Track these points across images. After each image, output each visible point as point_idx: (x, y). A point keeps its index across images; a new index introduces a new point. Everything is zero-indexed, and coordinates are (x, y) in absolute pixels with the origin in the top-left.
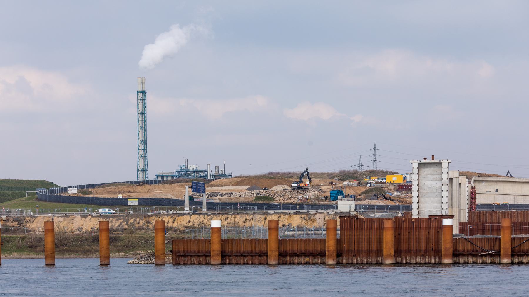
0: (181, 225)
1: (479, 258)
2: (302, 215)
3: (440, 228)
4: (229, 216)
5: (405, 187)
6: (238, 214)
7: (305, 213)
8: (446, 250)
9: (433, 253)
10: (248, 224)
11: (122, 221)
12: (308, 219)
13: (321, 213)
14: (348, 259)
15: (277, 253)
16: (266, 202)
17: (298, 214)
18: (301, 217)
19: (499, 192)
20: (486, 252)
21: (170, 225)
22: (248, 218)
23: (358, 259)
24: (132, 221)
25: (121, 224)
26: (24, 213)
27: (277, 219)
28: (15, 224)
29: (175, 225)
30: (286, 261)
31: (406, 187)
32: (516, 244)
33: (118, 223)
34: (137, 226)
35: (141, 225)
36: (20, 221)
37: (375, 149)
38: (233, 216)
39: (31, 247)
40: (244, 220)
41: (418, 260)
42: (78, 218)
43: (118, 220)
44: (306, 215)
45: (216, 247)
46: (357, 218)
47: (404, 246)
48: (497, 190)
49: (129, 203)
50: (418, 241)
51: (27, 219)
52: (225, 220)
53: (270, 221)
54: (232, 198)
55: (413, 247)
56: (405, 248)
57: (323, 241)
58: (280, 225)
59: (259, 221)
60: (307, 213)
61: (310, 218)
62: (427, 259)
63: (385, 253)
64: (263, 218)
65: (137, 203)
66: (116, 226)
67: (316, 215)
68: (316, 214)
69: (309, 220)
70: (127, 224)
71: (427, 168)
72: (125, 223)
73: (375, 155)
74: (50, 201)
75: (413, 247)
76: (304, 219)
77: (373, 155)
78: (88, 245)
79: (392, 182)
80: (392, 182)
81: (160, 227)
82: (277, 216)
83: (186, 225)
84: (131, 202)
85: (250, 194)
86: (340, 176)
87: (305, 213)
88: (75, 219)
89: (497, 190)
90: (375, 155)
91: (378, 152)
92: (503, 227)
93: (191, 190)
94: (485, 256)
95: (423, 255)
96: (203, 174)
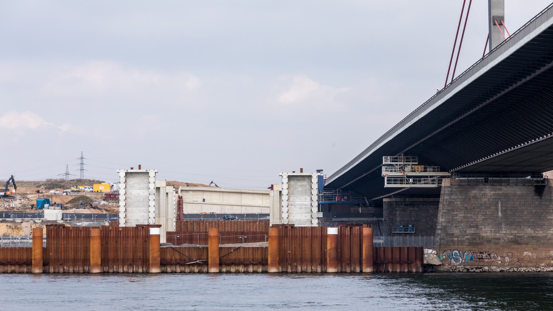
2: (8, 224)
5: (112, 196)
12: (14, 227)
13: (27, 221)
14: (54, 268)
17: (4, 223)
18: (7, 226)
20: (194, 261)
31: (113, 196)
37: (82, 158)
44: (12, 224)
56: (112, 257)
60: (13, 222)
61: (16, 227)
67: (22, 224)
68: (22, 222)
69: (15, 228)
71: (134, 177)
73: (82, 164)
75: (121, 255)
76: (10, 227)
77: (80, 164)
80: (99, 191)
86: (47, 185)
90: (82, 164)
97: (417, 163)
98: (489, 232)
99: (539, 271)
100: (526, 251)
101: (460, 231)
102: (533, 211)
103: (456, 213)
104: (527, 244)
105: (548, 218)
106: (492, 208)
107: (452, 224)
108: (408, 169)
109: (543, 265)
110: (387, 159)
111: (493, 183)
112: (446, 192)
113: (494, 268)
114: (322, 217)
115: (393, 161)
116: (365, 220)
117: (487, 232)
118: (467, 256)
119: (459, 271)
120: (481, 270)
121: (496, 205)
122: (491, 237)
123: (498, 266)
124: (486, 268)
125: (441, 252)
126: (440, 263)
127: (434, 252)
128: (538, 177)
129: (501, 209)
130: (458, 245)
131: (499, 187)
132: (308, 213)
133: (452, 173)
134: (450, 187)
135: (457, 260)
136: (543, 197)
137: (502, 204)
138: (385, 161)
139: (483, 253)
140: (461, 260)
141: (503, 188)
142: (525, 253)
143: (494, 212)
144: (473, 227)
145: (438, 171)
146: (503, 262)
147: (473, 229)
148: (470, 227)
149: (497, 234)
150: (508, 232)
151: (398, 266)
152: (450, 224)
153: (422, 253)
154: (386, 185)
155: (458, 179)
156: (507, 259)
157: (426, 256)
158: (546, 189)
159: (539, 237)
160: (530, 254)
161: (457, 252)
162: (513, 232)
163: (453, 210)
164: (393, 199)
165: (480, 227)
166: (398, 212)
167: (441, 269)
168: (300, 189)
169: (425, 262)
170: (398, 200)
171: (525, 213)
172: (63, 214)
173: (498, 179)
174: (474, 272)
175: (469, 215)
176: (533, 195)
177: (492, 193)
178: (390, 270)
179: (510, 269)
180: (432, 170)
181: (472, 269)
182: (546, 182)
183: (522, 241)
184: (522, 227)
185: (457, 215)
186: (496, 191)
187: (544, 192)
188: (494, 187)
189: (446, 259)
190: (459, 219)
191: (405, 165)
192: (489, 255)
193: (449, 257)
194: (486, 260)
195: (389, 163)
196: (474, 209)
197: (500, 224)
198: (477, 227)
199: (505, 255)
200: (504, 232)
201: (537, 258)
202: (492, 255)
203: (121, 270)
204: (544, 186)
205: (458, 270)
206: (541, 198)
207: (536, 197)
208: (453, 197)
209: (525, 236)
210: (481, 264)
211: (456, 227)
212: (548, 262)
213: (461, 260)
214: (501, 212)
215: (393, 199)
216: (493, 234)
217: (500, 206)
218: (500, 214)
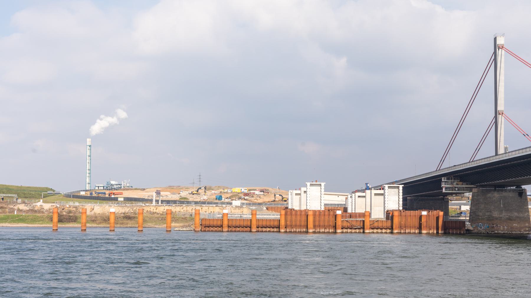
0: (160, 211)
1: (353, 230)
3: (448, 216)
4: (184, 207)
7: (221, 206)
11: (130, 208)
13: (229, 206)
14: (289, 229)
15: (256, 226)
16: (185, 200)
19: (338, 196)
20: (356, 227)
21: (155, 211)
22: (193, 208)
23: (294, 229)
24: (135, 208)
25: (129, 210)
26: (75, 204)
28: (74, 209)
29: (157, 211)
30: (259, 230)
33: (128, 209)
36: (76, 207)
37: (200, 176)
38: (186, 207)
40: (157, 209)
43: (128, 208)
47: (317, 223)
49: (119, 200)
50: (324, 221)
51: (80, 207)
52: (182, 209)
55: (322, 224)
56: (317, 225)
58: (145, 211)
60: (222, 206)
62: (327, 230)
65: (123, 200)
66: (127, 211)
68: (226, 207)
70: (132, 210)
71: (314, 186)
72: (132, 210)
75: (322, 224)
76: (221, 209)
79: (235, 192)
80: (235, 192)
82: (207, 207)
83: (163, 211)
84: (119, 199)
85: (177, 196)
87: (221, 206)
88: (106, 207)
92: (395, 215)
93: (156, 194)
94: (356, 229)
96: (119, 186)
97: (459, 181)
98: (497, 214)
99: (522, 234)
100: (515, 224)
101: (483, 214)
102: (518, 204)
103: (480, 205)
104: (515, 220)
105: (525, 208)
106: (498, 203)
107: (478, 211)
108: (455, 184)
109: (523, 230)
110: (444, 179)
111: (498, 191)
112: (475, 195)
113: (500, 232)
114: (123, 200)
115: (448, 180)
116: (245, 202)
117: (496, 214)
118: (486, 226)
119: (483, 233)
120: (494, 232)
121: (500, 201)
122: (497, 217)
123: (502, 231)
124: (496, 232)
125: (473, 224)
126: (473, 229)
127: (470, 224)
128: (520, 188)
129: (503, 203)
130: (481, 220)
131: (501, 193)
132: (397, 204)
133: (477, 186)
134: (477, 192)
135: (481, 228)
136: (522, 198)
137: (503, 201)
138: (444, 180)
139: (494, 224)
140: (483, 227)
141: (503, 193)
142: (514, 225)
143: (499, 205)
144: (489, 212)
145: (469, 185)
146: (504, 229)
147: (489, 213)
148: (488, 212)
149: (501, 216)
150: (506, 214)
151: (455, 230)
152: (477, 210)
153: (465, 225)
154: (444, 191)
155: (481, 188)
156: (506, 228)
157: (466, 225)
158: (524, 194)
159: (520, 217)
160: (516, 225)
161: (481, 224)
162: (508, 214)
163: (479, 204)
164: (413, 198)
165: (492, 212)
166: (415, 204)
167: (474, 232)
168: (393, 193)
169: (466, 228)
170: (415, 198)
171: (514, 205)
172: (241, 203)
173: (501, 189)
174: (491, 233)
175: (487, 206)
176: (517, 197)
177: (498, 195)
178: (451, 232)
179: (508, 232)
180: (465, 184)
181: (490, 232)
182: (524, 190)
183: (513, 219)
184: (512, 212)
185: (481, 206)
186: (500, 195)
187: (523, 195)
188: (499, 193)
189: (476, 227)
190: (482, 208)
191: (453, 182)
192: (497, 225)
193: (477, 226)
194: (496, 228)
195: (446, 181)
196: (489, 203)
197: (502, 210)
198: (491, 212)
199: (504, 225)
200: (504, 214)
201: (520, 227)
202: (498, 226)
203: (292, 231)
204: (523, 192)
205: (482, 232)
206: (521, 198)
207: (519, 198)
208: (479, 197)
209: (514, 217)
210: (493, 229)
211: (480, 212)
212: (525, 229)
213: (483, 227)
214: (503, 205)
215: (413, 198)
216: (499, 215)
217: (502, 202)
218: (502, 206)
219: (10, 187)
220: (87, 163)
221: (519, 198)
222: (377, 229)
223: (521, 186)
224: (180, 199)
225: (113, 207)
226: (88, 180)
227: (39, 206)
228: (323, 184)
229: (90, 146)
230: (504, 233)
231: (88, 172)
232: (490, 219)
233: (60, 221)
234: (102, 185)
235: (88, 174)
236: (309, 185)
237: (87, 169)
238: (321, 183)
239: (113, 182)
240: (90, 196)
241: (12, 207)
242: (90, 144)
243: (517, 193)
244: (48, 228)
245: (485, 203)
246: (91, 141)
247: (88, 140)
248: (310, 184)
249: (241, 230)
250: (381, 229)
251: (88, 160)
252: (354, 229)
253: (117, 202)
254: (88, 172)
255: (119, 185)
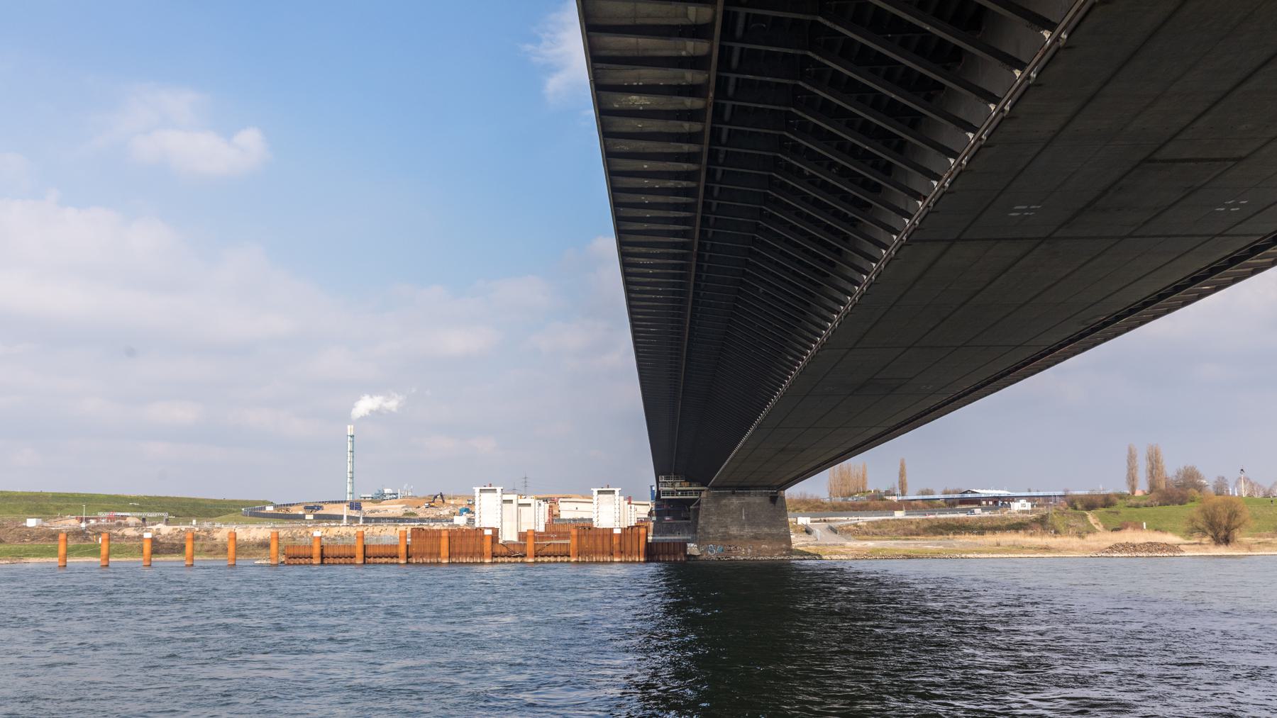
6: (376, 525)
8: (487, 553)
9: (478, 555)
10: (382, 533)
14: (416, 560)
19: (579, 509)
24: (295, 531)
25: (287, 533)
27: (405, 529)
28: (205, 534)
29: (328, 534)
32: (538, 548)
33: (285, 533)
34: (298, 534)
35: (302, 534)
39: (208, 551)
40: (380, 530)
41: (468, 560)
42: (255, 529)
45: (317, 551)
46: (423, 530)
48: (577, 508)
53: (400, 531)
54: (464, 513)
57: (397, 546)
59: (391, 531)
63: (442, 555)
64: (394, 528)
65: (312, 518)
74: (250, 516)
78: (253, 549)
81: (360, 535)
82: (405, 527)
89: (577, 508)
91: (528, 480)
94: (517, 557)
95: (471, 557)
104: (764, 539)
108: (678, 484)
117: (734, 530)
124: (733, 557)
127: (696, 546)
135: (712, 551)
142: (763, 546)
146: (746, 553)
148: (722, 527)
151: (667, 556)
156: (749, 551)
159: (773, 534)
167: (700, 558)
168: (607, 500)
169: (688, 553)
178: (661, 559)
189: (705, 550)
193: (707, 549)
197: (744, 525)
198: (726, 527)
202: (738, 548)
204: (777, 497)
208: (709, 505)
218: (744, 517)
219: (201, 502)
220: (349, 464)
221: (772, 505)
222: (549, 556)
223: (474, 488)
224: (405, 514)
225: (262, 529)
226: (349, 489)
227: (155, 530)
228: (617, 490)
229: (352, 436)
230: (745, 560)
231: (349, 476)
232: (726, 538)
233: (155, 552)
234: (370, 496)
235: (349, 479)
236: (479, 491)
237: (349, 471)
238: (496, 488)
239: (387, 491)
240: (276, 512)
241: (116, 532)
242: (352, 434)
243: (768, 498)
244: (139, 562)
245: (719, 513)
246: (354, 429)
247: (349, 427)
248: (598, 491)
249: (338, 562)
250: (556, 556)
251: (349, 458)
252: (514, 557)
253: (304, 521)
254: (349, 475)
255: (395, 494)
